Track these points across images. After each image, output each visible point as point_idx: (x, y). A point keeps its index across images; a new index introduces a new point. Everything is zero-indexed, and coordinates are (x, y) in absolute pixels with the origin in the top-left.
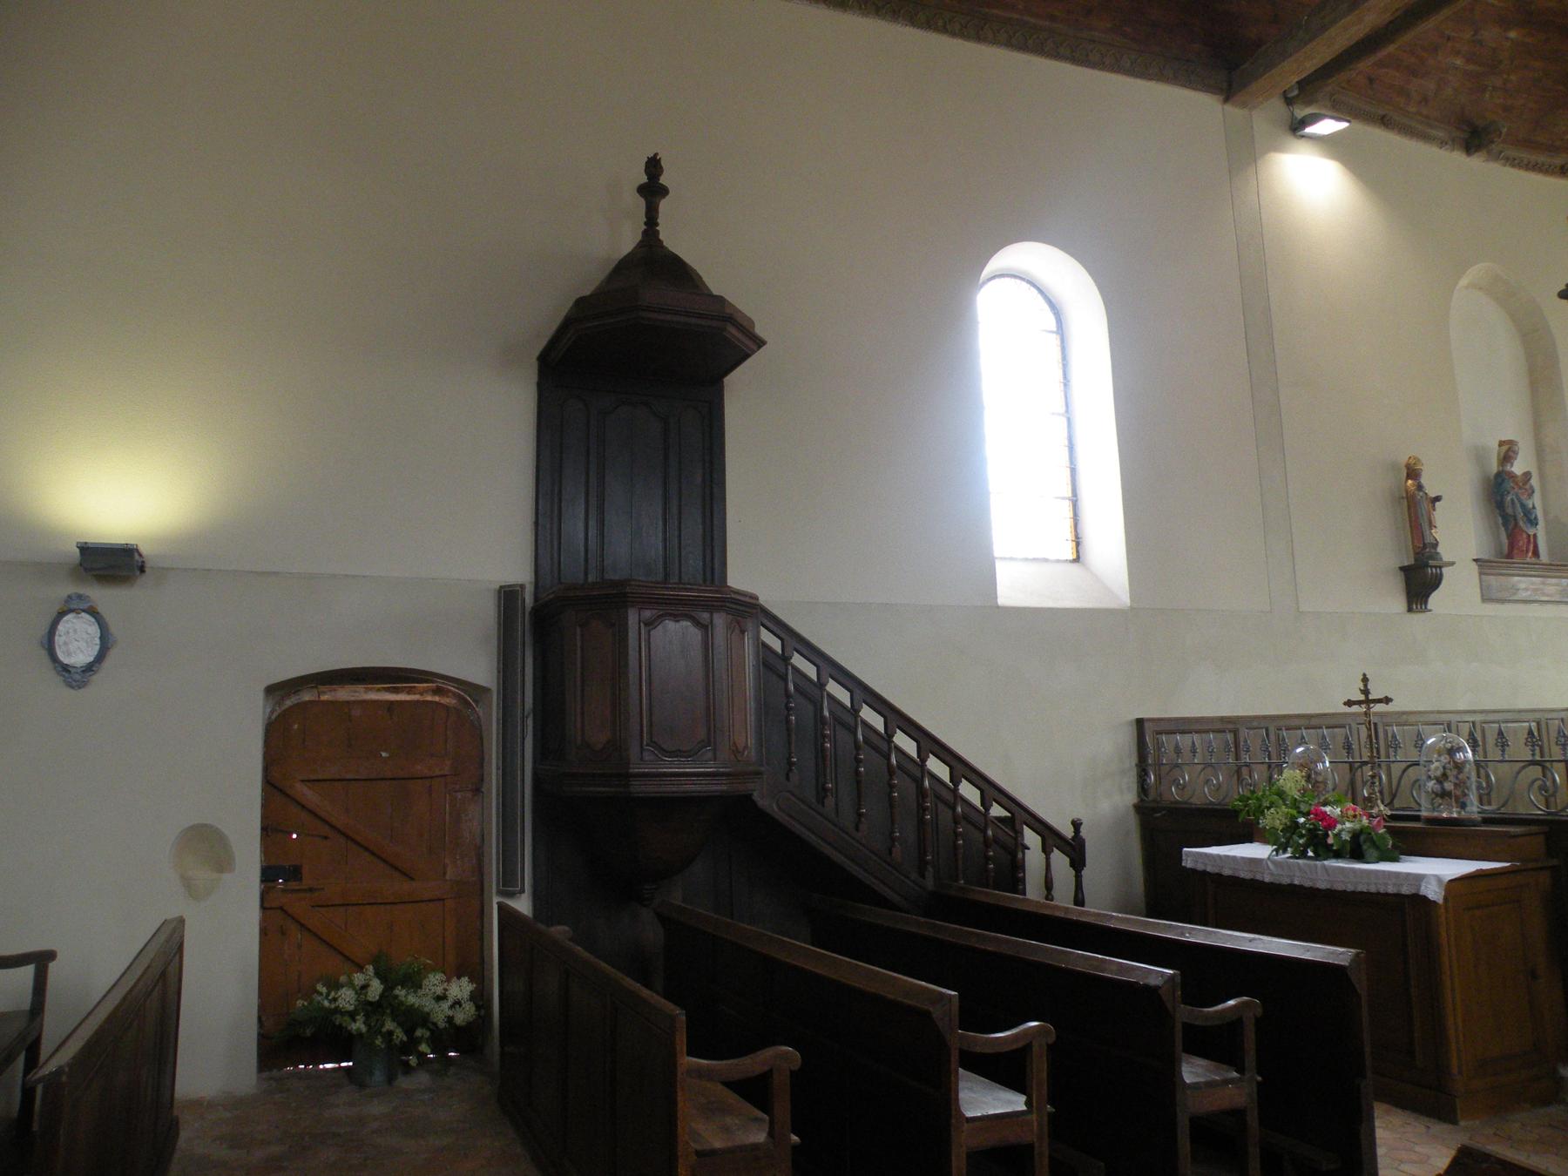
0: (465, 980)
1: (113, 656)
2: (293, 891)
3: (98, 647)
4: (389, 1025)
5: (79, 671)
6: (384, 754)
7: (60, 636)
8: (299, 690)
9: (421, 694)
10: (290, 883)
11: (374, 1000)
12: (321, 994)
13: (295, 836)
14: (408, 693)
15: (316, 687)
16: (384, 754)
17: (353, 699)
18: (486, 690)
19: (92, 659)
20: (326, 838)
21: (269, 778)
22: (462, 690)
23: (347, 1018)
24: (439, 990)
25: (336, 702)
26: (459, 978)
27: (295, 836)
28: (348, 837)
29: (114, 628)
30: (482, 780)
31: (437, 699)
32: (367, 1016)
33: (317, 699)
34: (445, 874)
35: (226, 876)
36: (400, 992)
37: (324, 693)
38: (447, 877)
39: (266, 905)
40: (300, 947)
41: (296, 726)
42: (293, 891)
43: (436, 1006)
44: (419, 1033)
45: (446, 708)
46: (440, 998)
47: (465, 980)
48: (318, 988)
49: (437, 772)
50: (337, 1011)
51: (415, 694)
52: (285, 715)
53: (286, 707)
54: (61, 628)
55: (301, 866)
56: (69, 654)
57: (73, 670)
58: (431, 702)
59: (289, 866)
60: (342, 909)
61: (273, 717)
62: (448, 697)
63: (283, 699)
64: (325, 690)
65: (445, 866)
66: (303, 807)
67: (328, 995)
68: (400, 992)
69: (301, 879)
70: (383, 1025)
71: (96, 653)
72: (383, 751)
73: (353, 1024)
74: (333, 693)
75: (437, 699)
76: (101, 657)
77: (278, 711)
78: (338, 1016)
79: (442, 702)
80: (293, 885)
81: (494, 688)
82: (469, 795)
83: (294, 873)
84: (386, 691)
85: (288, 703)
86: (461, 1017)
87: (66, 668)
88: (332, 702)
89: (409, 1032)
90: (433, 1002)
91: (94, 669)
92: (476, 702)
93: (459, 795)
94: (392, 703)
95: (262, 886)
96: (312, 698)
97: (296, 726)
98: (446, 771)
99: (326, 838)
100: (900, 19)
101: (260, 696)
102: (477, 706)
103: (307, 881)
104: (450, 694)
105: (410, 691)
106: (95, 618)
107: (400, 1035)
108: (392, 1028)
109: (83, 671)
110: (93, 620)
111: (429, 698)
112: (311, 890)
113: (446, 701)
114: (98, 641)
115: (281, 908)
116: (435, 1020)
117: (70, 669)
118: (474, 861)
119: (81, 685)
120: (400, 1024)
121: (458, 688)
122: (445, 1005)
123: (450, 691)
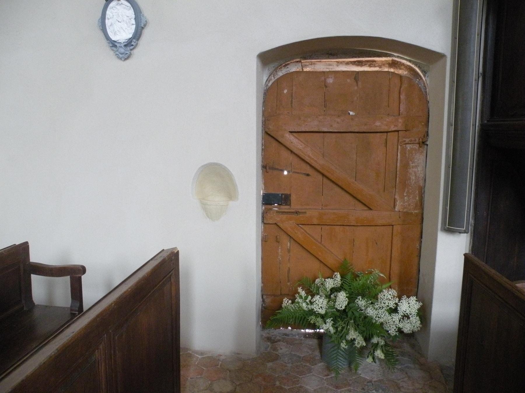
0: (413, 299)
1: (146, 33)
2: (283, 213)
3: (134, 26)
4: (353, 334)
5: (122, 45)
6: (351, 113)
7: (108, 19)
8: (288, 64)
9: (380, 67)
10: (282, 207)
11: (340, 309)
12: (301, 297)
13: (286, 173)
14: (370, 66)
15: (300, 61)
16: (351, 113)
17: (328, 70)
18: (439, 56)
19: (130, 36)
20: (308, 175)
21: (267, 130)
22: (414, 63)
23: (320, 320)
24: (392, 305)
25: (316, 72)
26: (408, 297)
27: (286, 173)
28: (323, 175)
29: (147, 13)
30: (428, 135)
31: (392, 70)
32: (335, 321)
33: (301, 70)
34: (394, 206)
35: (231, 203)
36: (361, 302)
37: (306, 66)
38: (397, 209)
39: (265, 221)
40: (289, 251)
41: (285, 91)
42: (283, 213)
43: (390, 318)
44: (375, 340)
45: (401, 77)
46: (394, 311)
47: (413, 299)
48: (299, 291)
49: (393, 128)
50: (312, 312)
51: (375, 67)
52: (278, 82)
53: (279, 77)
54: (109, 12)
55: (290, 195)
56: (115, 34)
57: (118, 45)
58: (388, 72)
59: (282, 194)
60: (319, 227)
61: (270, 84)
62: (400, 69)
63: (276, 70)
64: (308, 64)
65: (395, 201)
66: (292, 152)
67: (306, 298)
68: (361, 302)
69: (290, 205)
70: (348, 334)
71: (133, 31)
72: (351, 111)
73: (324, 325)
74: (313, 66)
75: (392, 70)
76: (137, 35)
77: (273, 80)
78: (313, 317)
79: (396, 72)
80: (285, 208)
81: (448, 52)
82: (416, 146)
83: (285, 200)
84: (353, 64)
85: (280, 74)
86: (407, 328)
87: (113, 44)
88: (312, 72)
89: (367, 339)
90: (387, 314)
91: (133, 43)
92: (425, 73)
93: (409, 147)
94: (358, 73)
95: (263, 208)
96: (298, 70)
97: (285, 91)
98: (400, 127)
99: (308, 175)
100: (402, 63)
101: (253, 63)
102: (425, 76)
103: (295, 205)
104: (402, 67)
105: (371, 64)
106: (131, 4)
107: (360, 342)
108: (355, 337)
109: (125, 46)
110: (129, 5)
111: (386, 69)
112: (297, 213)
113: (400, 72)
114: (133, 22)
115: (276, 224)
116: (388, 329)
117: (116, 44)
118: (417, 198)
119: (127, 57)
120: (361, 333)
121: (410, 61)
122: (396, 317)
123: (403, 64)
